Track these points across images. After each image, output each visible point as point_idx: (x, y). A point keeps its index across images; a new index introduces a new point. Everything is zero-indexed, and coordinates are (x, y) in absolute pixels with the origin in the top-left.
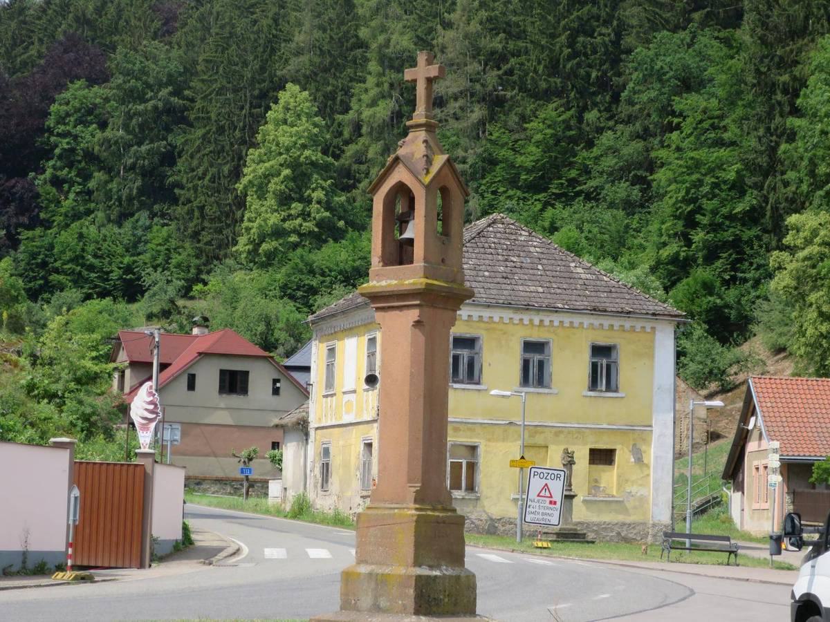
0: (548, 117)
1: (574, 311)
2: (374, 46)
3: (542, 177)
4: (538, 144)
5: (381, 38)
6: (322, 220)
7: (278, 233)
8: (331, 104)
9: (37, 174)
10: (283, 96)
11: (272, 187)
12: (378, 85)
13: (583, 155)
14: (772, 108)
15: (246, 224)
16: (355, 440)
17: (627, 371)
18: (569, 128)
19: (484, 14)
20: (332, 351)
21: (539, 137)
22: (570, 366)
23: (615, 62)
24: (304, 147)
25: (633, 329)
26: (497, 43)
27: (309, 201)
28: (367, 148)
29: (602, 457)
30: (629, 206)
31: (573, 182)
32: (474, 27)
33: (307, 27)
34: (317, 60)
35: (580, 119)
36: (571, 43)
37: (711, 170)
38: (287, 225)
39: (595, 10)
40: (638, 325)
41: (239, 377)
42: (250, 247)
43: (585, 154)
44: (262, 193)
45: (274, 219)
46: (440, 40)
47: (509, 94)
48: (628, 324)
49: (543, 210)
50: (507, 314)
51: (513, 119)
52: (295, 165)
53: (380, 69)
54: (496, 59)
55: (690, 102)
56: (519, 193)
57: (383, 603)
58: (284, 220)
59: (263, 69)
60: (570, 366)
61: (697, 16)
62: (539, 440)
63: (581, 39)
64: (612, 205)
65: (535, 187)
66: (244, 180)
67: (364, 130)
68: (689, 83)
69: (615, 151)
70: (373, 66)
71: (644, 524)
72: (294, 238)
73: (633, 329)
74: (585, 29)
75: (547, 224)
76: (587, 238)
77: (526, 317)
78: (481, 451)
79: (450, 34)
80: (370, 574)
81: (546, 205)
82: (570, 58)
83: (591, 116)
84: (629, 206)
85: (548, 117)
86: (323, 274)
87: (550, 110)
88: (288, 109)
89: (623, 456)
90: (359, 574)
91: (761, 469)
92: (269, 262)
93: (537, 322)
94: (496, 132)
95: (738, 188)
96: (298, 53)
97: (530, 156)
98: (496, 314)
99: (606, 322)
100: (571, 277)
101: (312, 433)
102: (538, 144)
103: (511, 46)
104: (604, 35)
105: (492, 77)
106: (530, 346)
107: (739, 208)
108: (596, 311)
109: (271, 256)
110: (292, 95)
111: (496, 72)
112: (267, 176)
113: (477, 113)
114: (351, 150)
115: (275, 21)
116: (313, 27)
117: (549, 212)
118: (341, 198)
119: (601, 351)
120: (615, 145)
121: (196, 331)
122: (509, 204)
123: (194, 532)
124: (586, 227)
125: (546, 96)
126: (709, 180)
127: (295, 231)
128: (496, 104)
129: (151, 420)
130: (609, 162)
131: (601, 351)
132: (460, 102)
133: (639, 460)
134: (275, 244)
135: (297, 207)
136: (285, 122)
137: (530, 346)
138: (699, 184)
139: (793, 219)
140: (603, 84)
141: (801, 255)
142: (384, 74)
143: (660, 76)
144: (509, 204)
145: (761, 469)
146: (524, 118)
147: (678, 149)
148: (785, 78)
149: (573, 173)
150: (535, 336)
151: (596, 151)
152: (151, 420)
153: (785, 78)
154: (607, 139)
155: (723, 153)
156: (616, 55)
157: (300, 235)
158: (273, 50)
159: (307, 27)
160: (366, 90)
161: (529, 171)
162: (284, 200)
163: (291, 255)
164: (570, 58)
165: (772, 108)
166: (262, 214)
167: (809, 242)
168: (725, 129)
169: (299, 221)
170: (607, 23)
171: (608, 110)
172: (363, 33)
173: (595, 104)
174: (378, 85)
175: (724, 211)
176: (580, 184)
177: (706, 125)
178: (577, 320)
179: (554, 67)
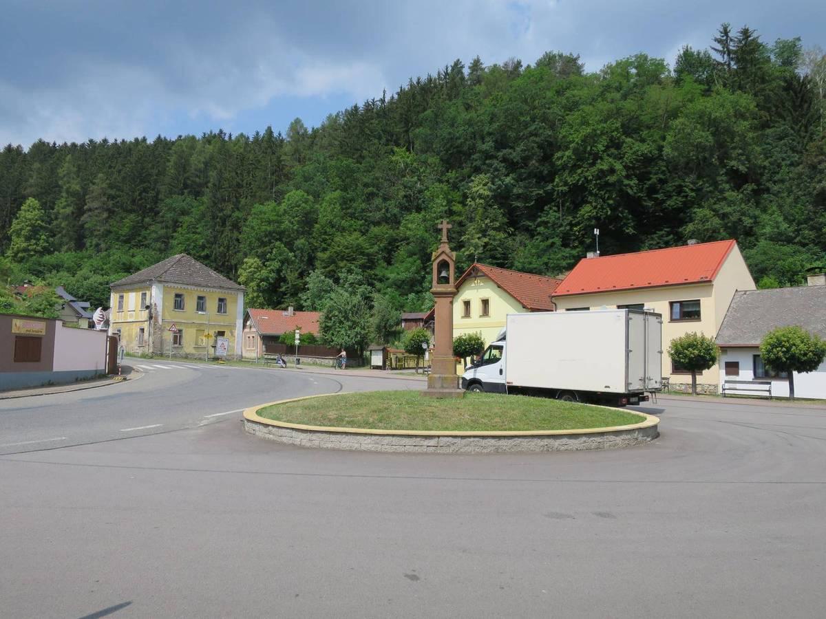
0: (130, 219)
1: (214, 287)
2: (65, 187)
3: (129, 239)
4: (127, 227)
5: (67, 185)
6: (45, 247)
7: (25, 250)
8: (47, 206)
9: (515, 229)
10: (28, 202)
11: (23, 233)
12: (66, 201)
13: (144, 232)
14: (216, 223)
15: (12, 246)
16: (135, 329)
17: (229, 306)
18: (138, 223)
19: (108, 181)
20: (122, 297)
21: (128, 225)
22: (212, 305)
23: (156, 203)
24: (37, 220)
25: (231, 294)
26: (112, 192)
27: (39, 240)
28: (61, 223)
29: (221, 334)
30: (161, 251)
31: (140, 241)
32: (104, 185)
33: (35, 177)
34: (39, 190)
35: (143, 221)
36: (140, 194)
37: (193, 241)
38: (29, 248)
39: (149, 185)
40: (233, 292)
41: (686, 310)
42: (13, 255)
43: (145, 232)
44: (19, 235)
45: (24, 245)
46: (91, 189)
47: (117, 210)
48: (230, 292)
49: (129, 249)
50: (193, 287)
51: (118, 219)
52: (33, 226)
53: (67, 196)
54: (112, 197)
55: (186, 219)
56: (120, 243)
57: (445, 385)
58: (28, 246)
59: (16, 191)
60: (212, 305)
61: (186, 191)
62: (202, 328)
63: (144, 194)
64: (154, 250)
65: (126, 242)
66: (11, 231)
67: (60, 216)
68: (184, 212)
69: (156, 232)
70: (64, 194)
71: (233, 355)
72: (32, 253)
73: (225, 293)
74: (145, 190)
75: (131, 254)
76: (146, 260)
77: (199, 289)
78: (184, 331)
79: (95, 187)
80: (440, 377)
81: (130, 248)
82: (139, 200)
83: (147, 220)
84: (161, 251)
85: (130, 219)
86: (44, 266)
87: (132, 216)
88: (30, 206)
89: (227, 333)
90: (435, 377)
91: (251, 337)
92: (21, 260)
93: (202, 290)
94: (111, 221)
95: (203, 247)
96: (31, 186)
97: (125, 231)
98: (189, 287)
99: (224, 291)
100: (211, 276)
101: (111, 325)
102: (127, 227)
103: (117, 193)
104: (152, 194)
105: (111, 203)
106: (177, 296)
107: (203, 254)
108: (221, 287)
109: (22, 259)
110: (31, 201)
111: (112, 202)
112: (21, 229)
113: (105, 215)
114: (55, 223)
115: (21, 174)
116: (37, 178)
117: (132, 251)
118: (51, 239)
119: (200, 298)
120: (156, 230)
121: (26, 286)
122: (117, 247)
123: (97, 367)
124: (146, 256)
125: (131, 211)
126: (193, 244)
127: (32, 250)
128: (111, 212)
129: (101, 321)
130: (154, 235)
131: (200, 298)
132: (98, 211)
133: (232, 335)
134: (24, 254)
135: (33, 241)
136: (28, 211)
137: (177, 296)
138: (189, 245)
139: (246, 260)
140: (151, 210)
141: (248, 271)
142: (68, 197)
143: (174, 209)
144: (117, 247)
145: (251, 337)
146: (122, 218)
147: (181, 234)
148: (221, 214)
149: (140, 238)
150: (201, 295)
151: (148, 231)
152: (101, 321)
153: (221, 214)
154: (152, 228)
155: (197, 236)
156: (156, 200)
157: (35, 252)
158: (20, 184)
159: (35, 177)
160: (61, 203)
161: (125, 236)
162: (28, 239)
163: (30, 259)
164: (139, 200)
165: (216, 223)
166: (19, 243)
167: (250, 267)
168: (197, 228)
169: (34, 247)
170: (153, 190)
171: (153, 218)
172: (60, 183)
173: (148, 216)
174: (66, 201)
175: (198, 254)
176: (142, 241)
177: (191, 227)
178: (215, 290)
179: (133, 201)
